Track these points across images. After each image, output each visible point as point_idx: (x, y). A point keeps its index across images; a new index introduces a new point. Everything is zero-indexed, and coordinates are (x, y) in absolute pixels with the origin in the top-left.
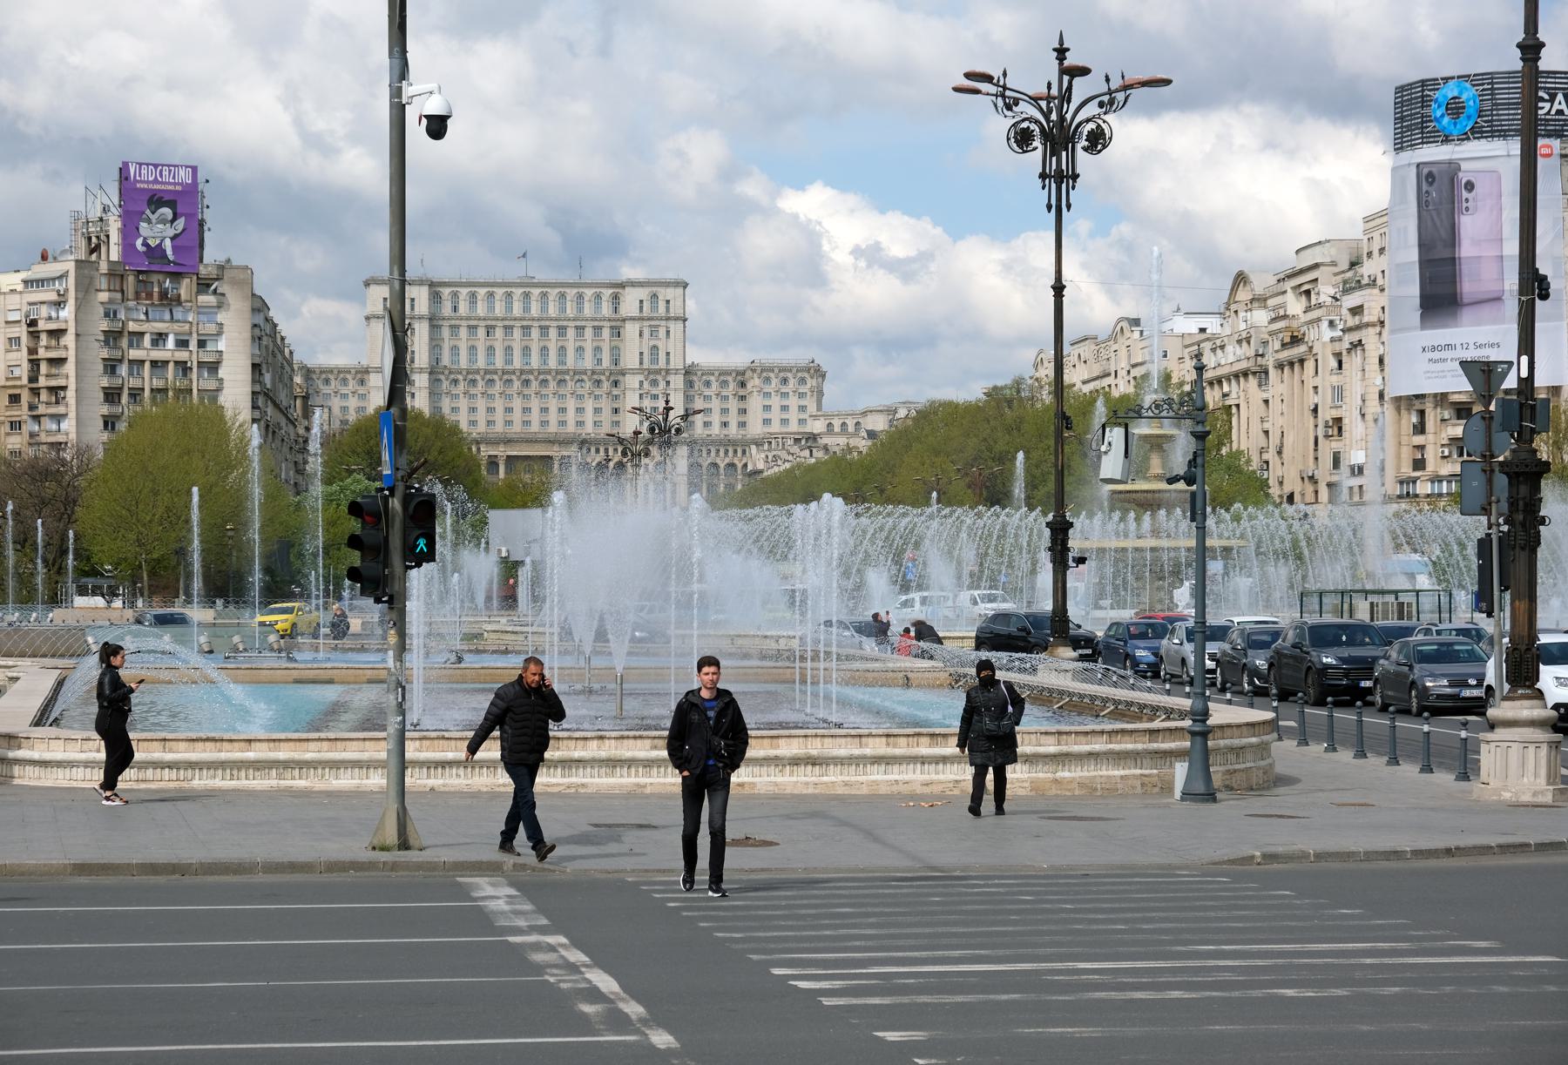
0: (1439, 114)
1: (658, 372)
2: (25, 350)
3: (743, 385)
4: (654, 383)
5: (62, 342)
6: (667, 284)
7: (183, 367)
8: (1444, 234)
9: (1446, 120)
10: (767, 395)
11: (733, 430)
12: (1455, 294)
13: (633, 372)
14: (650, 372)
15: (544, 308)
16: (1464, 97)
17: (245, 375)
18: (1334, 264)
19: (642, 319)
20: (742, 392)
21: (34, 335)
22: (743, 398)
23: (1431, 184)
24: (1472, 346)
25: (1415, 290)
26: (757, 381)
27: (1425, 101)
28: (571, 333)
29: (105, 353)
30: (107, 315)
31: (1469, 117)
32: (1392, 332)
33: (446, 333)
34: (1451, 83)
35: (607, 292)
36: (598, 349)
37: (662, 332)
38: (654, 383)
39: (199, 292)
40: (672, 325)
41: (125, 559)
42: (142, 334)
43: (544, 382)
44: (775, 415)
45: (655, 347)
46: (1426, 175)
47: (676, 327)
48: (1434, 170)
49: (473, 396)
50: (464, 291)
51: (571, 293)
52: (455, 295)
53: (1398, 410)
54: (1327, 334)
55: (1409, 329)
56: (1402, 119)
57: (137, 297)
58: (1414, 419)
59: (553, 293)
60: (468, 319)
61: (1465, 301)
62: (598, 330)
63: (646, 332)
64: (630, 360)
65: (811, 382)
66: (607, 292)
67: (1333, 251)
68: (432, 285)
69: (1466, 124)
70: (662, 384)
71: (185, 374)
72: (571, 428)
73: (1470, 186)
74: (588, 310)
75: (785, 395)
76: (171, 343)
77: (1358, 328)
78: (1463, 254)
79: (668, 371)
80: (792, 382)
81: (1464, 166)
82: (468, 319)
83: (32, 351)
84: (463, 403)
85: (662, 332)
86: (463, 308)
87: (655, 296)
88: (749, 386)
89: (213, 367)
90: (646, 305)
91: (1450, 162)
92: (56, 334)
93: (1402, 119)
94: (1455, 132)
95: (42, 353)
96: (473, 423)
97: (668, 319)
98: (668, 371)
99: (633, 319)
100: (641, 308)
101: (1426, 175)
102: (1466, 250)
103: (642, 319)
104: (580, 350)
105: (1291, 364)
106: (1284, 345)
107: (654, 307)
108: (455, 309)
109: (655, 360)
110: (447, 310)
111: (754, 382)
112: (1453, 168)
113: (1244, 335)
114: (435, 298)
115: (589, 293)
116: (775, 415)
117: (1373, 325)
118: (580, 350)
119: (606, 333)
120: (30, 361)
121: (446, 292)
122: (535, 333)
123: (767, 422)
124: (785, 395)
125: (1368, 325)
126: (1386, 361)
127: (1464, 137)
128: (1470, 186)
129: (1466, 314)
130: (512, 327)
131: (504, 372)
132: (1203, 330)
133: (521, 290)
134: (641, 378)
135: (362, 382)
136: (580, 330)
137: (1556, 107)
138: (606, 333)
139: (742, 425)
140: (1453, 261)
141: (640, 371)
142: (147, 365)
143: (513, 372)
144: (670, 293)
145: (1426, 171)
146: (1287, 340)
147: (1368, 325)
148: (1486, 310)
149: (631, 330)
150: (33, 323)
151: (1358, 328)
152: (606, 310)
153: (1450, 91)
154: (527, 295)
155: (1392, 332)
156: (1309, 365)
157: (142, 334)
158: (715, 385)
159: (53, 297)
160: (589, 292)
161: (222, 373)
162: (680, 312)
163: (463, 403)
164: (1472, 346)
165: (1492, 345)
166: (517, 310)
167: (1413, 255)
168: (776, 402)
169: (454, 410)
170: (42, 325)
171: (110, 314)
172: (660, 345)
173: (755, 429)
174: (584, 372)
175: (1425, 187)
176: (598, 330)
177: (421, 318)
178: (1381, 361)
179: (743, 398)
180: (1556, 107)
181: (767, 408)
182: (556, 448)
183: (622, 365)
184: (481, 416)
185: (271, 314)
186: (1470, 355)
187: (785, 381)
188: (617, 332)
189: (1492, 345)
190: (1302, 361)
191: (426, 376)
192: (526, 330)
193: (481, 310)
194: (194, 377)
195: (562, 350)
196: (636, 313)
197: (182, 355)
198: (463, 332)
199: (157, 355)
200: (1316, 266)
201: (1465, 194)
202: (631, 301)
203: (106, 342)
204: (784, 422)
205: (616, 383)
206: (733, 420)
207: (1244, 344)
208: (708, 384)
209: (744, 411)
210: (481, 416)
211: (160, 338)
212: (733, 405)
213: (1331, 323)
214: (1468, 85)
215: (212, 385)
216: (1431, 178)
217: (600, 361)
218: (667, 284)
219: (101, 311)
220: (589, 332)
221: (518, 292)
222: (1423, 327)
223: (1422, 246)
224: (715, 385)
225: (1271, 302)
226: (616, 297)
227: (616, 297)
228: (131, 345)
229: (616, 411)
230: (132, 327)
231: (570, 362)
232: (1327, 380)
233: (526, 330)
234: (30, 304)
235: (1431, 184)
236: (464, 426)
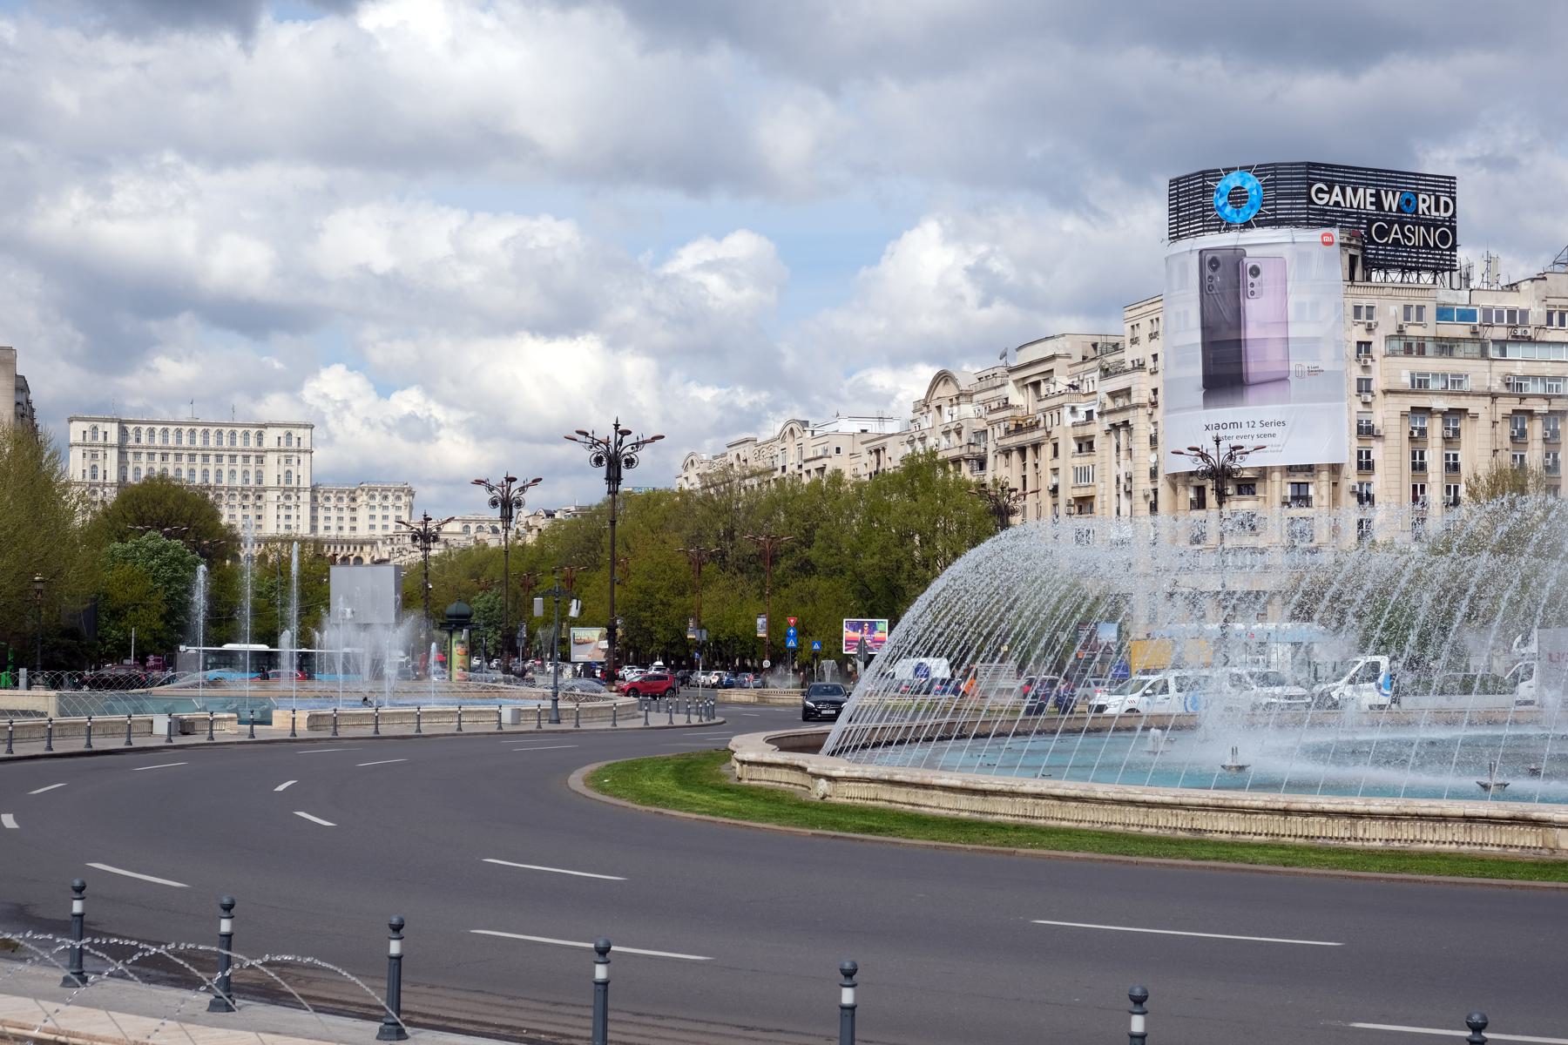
0: (1221, 203)
1: (291, 489)
3: (354, 500)
4: (288, 497)
6: (299, 426)
8: (1227, 315)
9: (1228, 209)
10: (373, 507)
11: (346, 533)
12: (1241, 374)
13: (273, 489)
14: (285, 489)
15: (206, 442)
16: (1247, 187)
18: (1068, 356)
22: (354, 510)
23: (1214, 269)
24: (1258, 424)
25: (1197, 371)
26: (365, 498)
27: (1206, 191)
28: (226, 460)
31: (1252, 207)
32: (1168, 411)
33: (130, 457)
34: (1233, 174)
35: (253, 431)
36: (246, 472)
37: (295, 460)
38: (288, 497)
40: (302, 456)
41: (507, 670)
44: (378, 522)
45: (289, 472)
46: (1211, 263)
47: (305, 458)
48: (1218, 256)
50: (145, 428)
51: (226, 431)
52: (138, 430)
53: (1175, 489)
54: (1068, 419)
55: (1191, 408)
56: (1178, 210)
58: (1192, 495)
59: (212, 430)
61: (1252, 379)
62: (246, 458)
64: (270, 480)
65: (405, 499)
66: (253, 431)
67: (1068, 345)
68: (121, 422)
69: (1248, 213)
70: (294, 498)
73: (1255, 271)
74: (239, 444)
75: (386, 508)
77: (1124, 409)
78: (1249, 336)
80: (391, 498)
81: (1249, 252)
85: (295, 460)
86: (144, 440)
87: (289, 434)
88: (359, 501)
90: (283, 441)
91: (1235, 248)
93: (1178, 210)
94: (1238, 221)
101: (1211, 263)
102: (1252, 332)
104: (233, 472)
105: (1022, 450)
106: (1008, 432)
107: (289, 443)
108: (138, 440)
109: (288, 481)
110: (132, 442)
111: (362, 498)
112: (1238, 254)
113: (953, 426)
114: (123, 432)
115: (240, 431)
116: (378, 522)
117: (1143, 406)
118: (233, 472)
119: (252, 460)
121: (130, 428)
123: (372, 527)
124: (386, 508)
125: (1137, 406)
126: (1160, 440)
127: (1247, 225)
128: (1255, 271)
129: (1252, 394)
131: (229, 489)
132: (864, 431)
136: (233, 458)
137: (1334, 198)
138: (252, 460)
139: (354, 529)
140: (1238, 343)
141: (278, 489)
144: (301, 432)
145: (1209, 257)
146: (1012, 428)
147: (1137, 406)
148: (1271, 391)
149: (271, 459)
151: (1124, 409)
152: (253, 444)
153: (1233, 180)
154: (193, 432)
155: (1168, 411)
156: (1047, 450)
158: (333, 500)
160: (240, 431)
162: (308, 447)
164: (1258, 424)
165: (1278, 424)
166: (185, 442)
167: (1197, 337)
168: (378, 512)
172: (293, 470)
174: (236, 489)
175: (1208, 272)
176: (246, 458)
177: (112, 446)
179: (354, 510)
180: (1334, 198)
181: (372, 517)
183: (265, 484)
185: (31, 397)
187: (386, 497)
188: (260, 460)
189: (1278, 424)
190: (1036, 447)
192: (192, 457)
193: (158, 441)
195: (219, 472)
198: (144, 457)
200: (1053, 357)
201: (1250, 279)
202: (271, 438)
204: (385, 527)
205: (259, 497)
206: (347, 524)
207: (953, 436)
208: (328, 499)
209: (354, 519)
212: (346, 514)
213: (1073, 410)
214: (1251, 175)
216: (1214, 263)
217: (247, 481)
218: (299, 426)
221: (186, 429)
222: (1206, 405)
223: (1205, 328)
224: (333, 500)
225: (975, 398)
227: (260, 434)
229: (259, 517)
231: (225, 481)
232: (1070, 459)
233: (192, 457)
235: (1214, 269)
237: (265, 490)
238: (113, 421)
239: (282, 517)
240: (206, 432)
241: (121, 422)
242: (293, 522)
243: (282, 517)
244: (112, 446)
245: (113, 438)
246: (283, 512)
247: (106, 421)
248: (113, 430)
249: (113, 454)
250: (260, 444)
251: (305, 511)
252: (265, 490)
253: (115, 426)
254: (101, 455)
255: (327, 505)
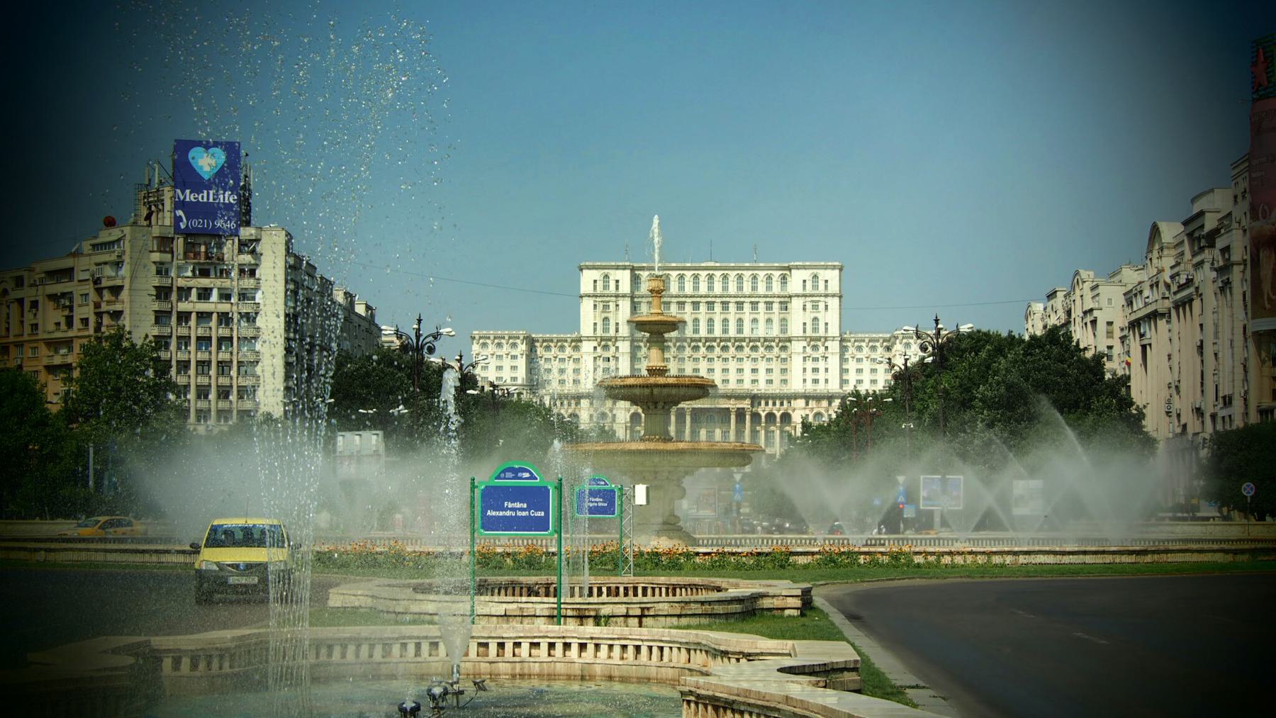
1: (818, 339)
2: (92, 305)
4: (815, 348)
5: (120, 298)
7: (225, 319)
13: (798, 339)
14: (812, 339)
17: (279, 324)
19: (805, 296)
20: (784, 355)
21: (99, 291)
28: (747, 307)
29: (156, 306)
30: (159, 272)
37: (822, 306)
39: (240, 252)
42: (190, 289)
43: (696, 348)
45: (816, 319)
49: (726, 360)
57: (186, 256)
60: (766, 296)
63: (809, 306)
64: (795, 329)
70: (822, 349)
71: (227, 324)
72: (747, 385)
76: (215, 296)
79: (826, 339)
82: (766, 296)
83: (97, 305)
84: (718, 365)
85: (822, 306)
87: (815, 277)
89: (250, 318)
90: (809, 284)
92: (116, 290)
95: (104, 307)
96: (725, 381)
97: (826, 296)
98: (826, 339)
99: (798, 296)
100: (804, 287)
103: (805, 296)
104: (769, 321)
109: (815, 330)
114: (635, 280)
119: (776, 306)
120: (96, 314)
122: (718, 308)
130: (684, 303)
133: (706, 272)
134: (805, 344)
135: (576, 348)
138: (776, 306)
139: (785, 381)
142: (194, 316)
143: (685, 340)
149: (796, 304)
150: (97, 281)
157: (190, 289)
159: (113, 257)
161: (260, 322)
163: (718, 365)
169: (711, 370)
170: (105, 283)
171: (162, 270)
172: (611, 316)
173: (796, 386)
177: (624, 296)
178: (1201, 325)
179: (785, 360)
182: (732, 401)
184: (733, 376)
186: (236, 252)
188: (784, 307)
191: (627, 344)
192: (710, 305)
194: (235, 327)
196: (800, 291)
197: (224, 307)
199: (203, 307)
203: (158, 297)
206: (776, 376)
209: (576, 371)
210: (733, 376)
211: (204, 294)
215: (250, 333)
219: (153, 268)
220: (762, 306)
226: (784, 278)
227: (784, 278)
228: (179, 299)
230: (181, 282)
231: (747, 332)
234: (97, 264)
236: (718, 382)
237: (789, 340)
238: (624, 268)
239: (809, 370)
240: (769, 278)
241: (633, 269)
242: (821, 376)
243: (809, 370)
244: (624, 296)
245: (625, 288)
246: (810, 365)
247: (617, 268)
248: (624, 277)
249: (625, 305)
250: (617, 288)
251: (834, 361)
252: (789, 340)
253: (628, 272)
254: (612, 305)
255: (725, 355)
